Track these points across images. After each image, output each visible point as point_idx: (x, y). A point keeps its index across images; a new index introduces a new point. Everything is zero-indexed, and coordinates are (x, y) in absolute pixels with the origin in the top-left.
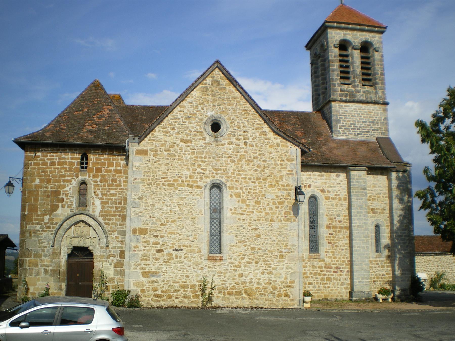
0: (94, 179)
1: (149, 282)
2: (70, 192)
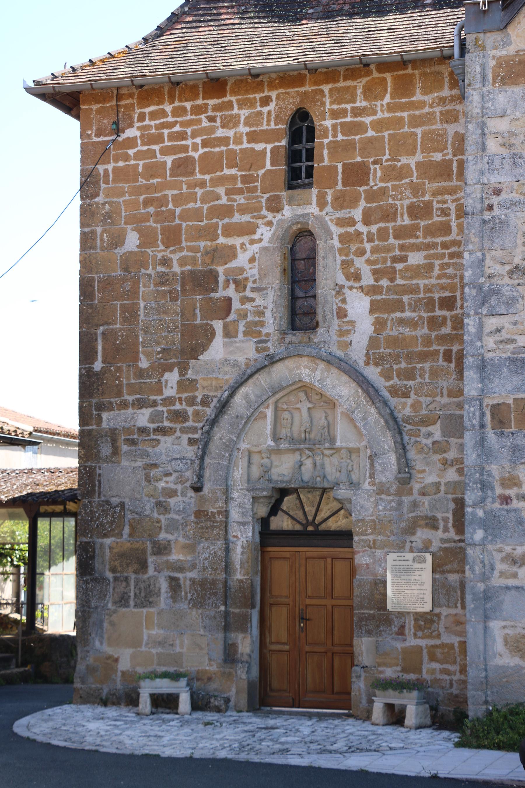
0: (339, 214)
2: (252, 272)
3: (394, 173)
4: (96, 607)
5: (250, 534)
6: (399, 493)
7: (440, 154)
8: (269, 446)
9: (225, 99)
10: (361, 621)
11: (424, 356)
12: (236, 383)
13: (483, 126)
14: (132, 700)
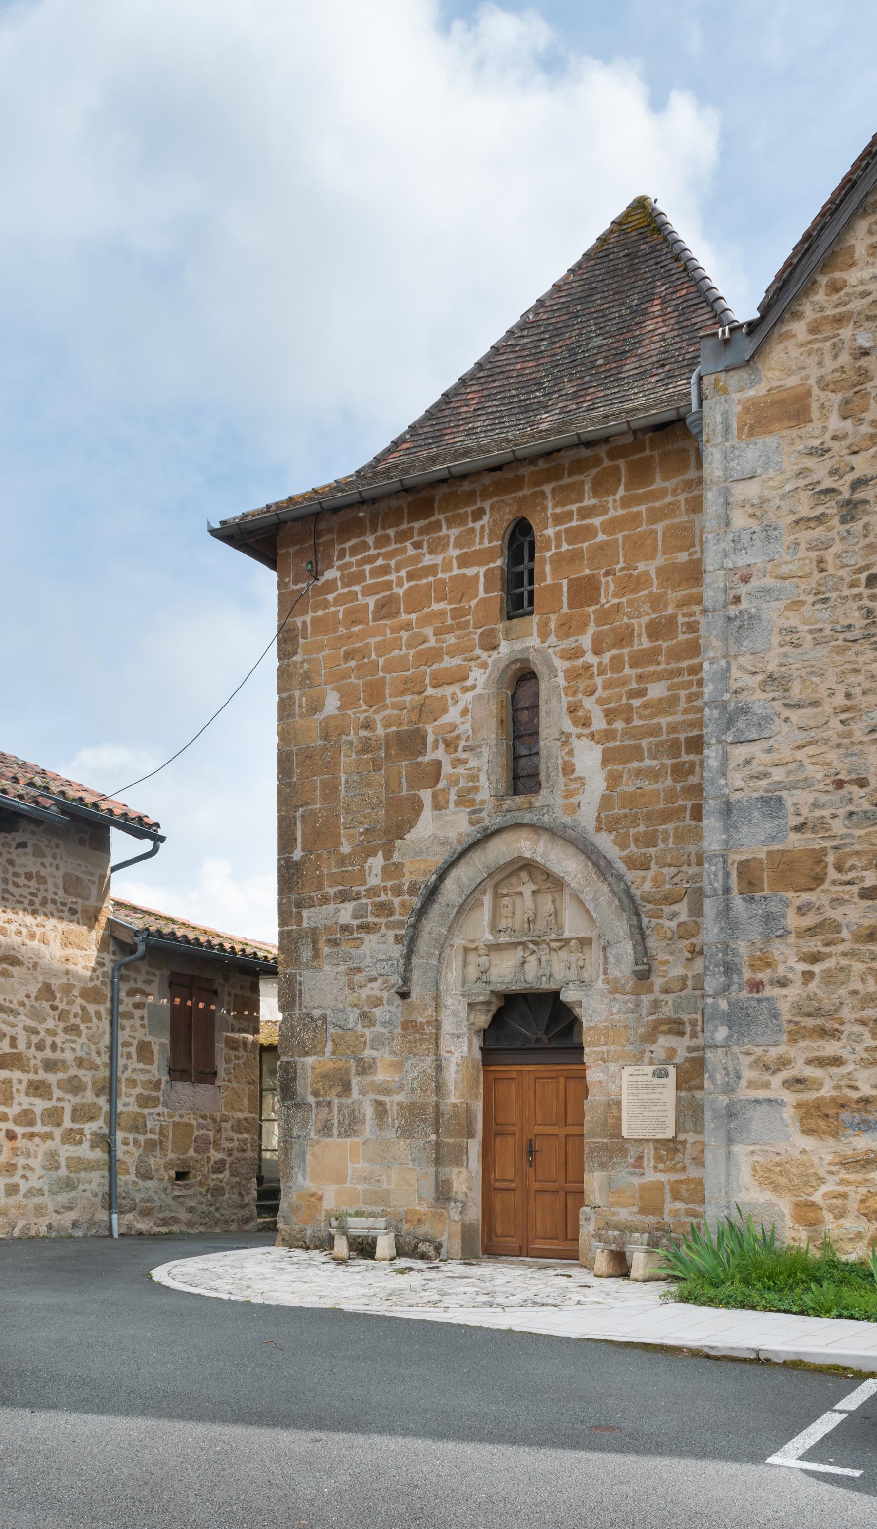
0: (565, 644)
1: (846, 1163)
2: (465, 728)
3: (631, 584)
4: (299, 1137)
5: (466, 1049)
6: (637, 992)
7: (687, 554)
8: (487, 940)
9: (433, 519)
10: (592, 1152)
11: (667, 816)
12: (445, 863)
13: (726, 493)
14: (325, 1244)
